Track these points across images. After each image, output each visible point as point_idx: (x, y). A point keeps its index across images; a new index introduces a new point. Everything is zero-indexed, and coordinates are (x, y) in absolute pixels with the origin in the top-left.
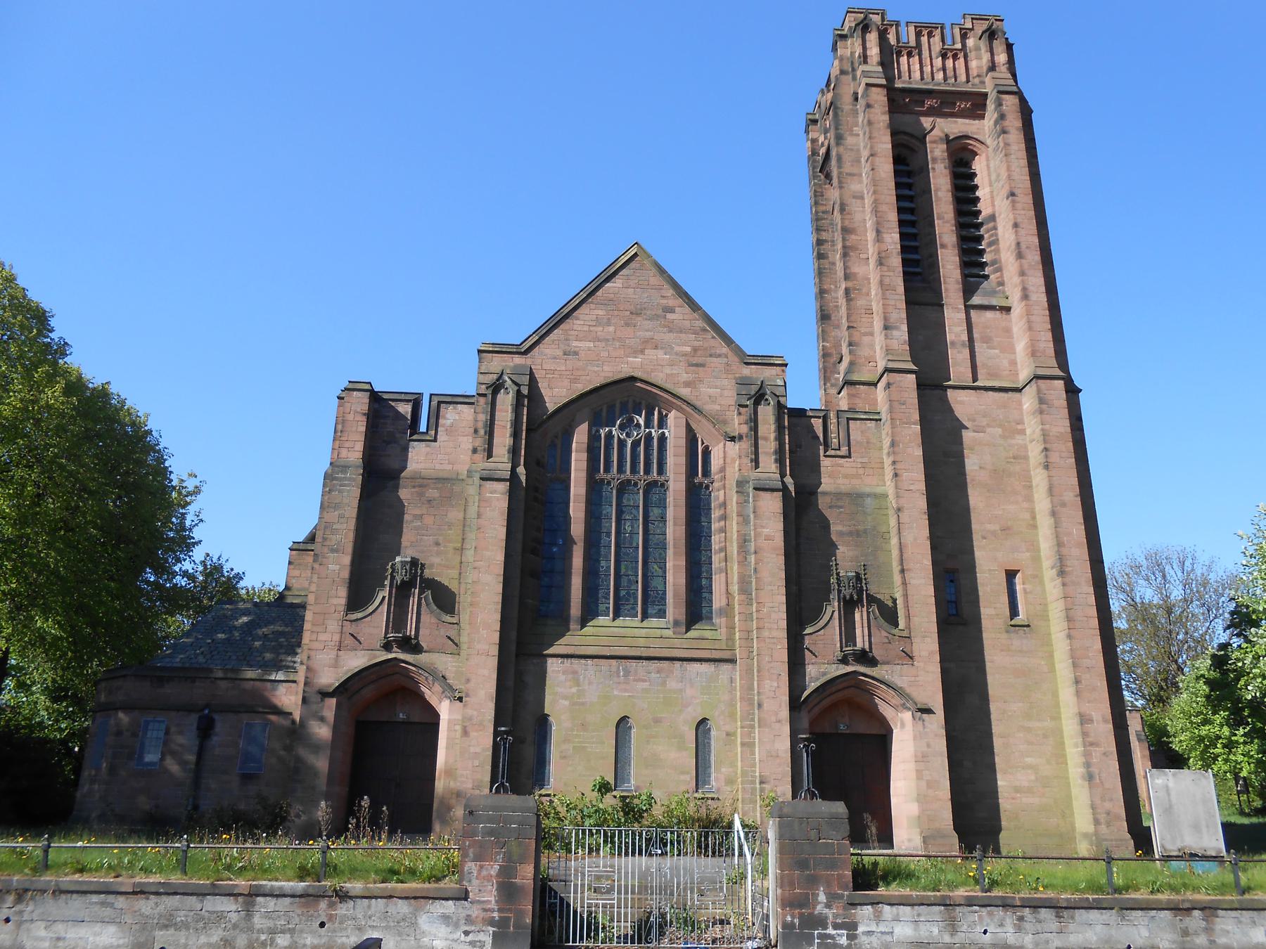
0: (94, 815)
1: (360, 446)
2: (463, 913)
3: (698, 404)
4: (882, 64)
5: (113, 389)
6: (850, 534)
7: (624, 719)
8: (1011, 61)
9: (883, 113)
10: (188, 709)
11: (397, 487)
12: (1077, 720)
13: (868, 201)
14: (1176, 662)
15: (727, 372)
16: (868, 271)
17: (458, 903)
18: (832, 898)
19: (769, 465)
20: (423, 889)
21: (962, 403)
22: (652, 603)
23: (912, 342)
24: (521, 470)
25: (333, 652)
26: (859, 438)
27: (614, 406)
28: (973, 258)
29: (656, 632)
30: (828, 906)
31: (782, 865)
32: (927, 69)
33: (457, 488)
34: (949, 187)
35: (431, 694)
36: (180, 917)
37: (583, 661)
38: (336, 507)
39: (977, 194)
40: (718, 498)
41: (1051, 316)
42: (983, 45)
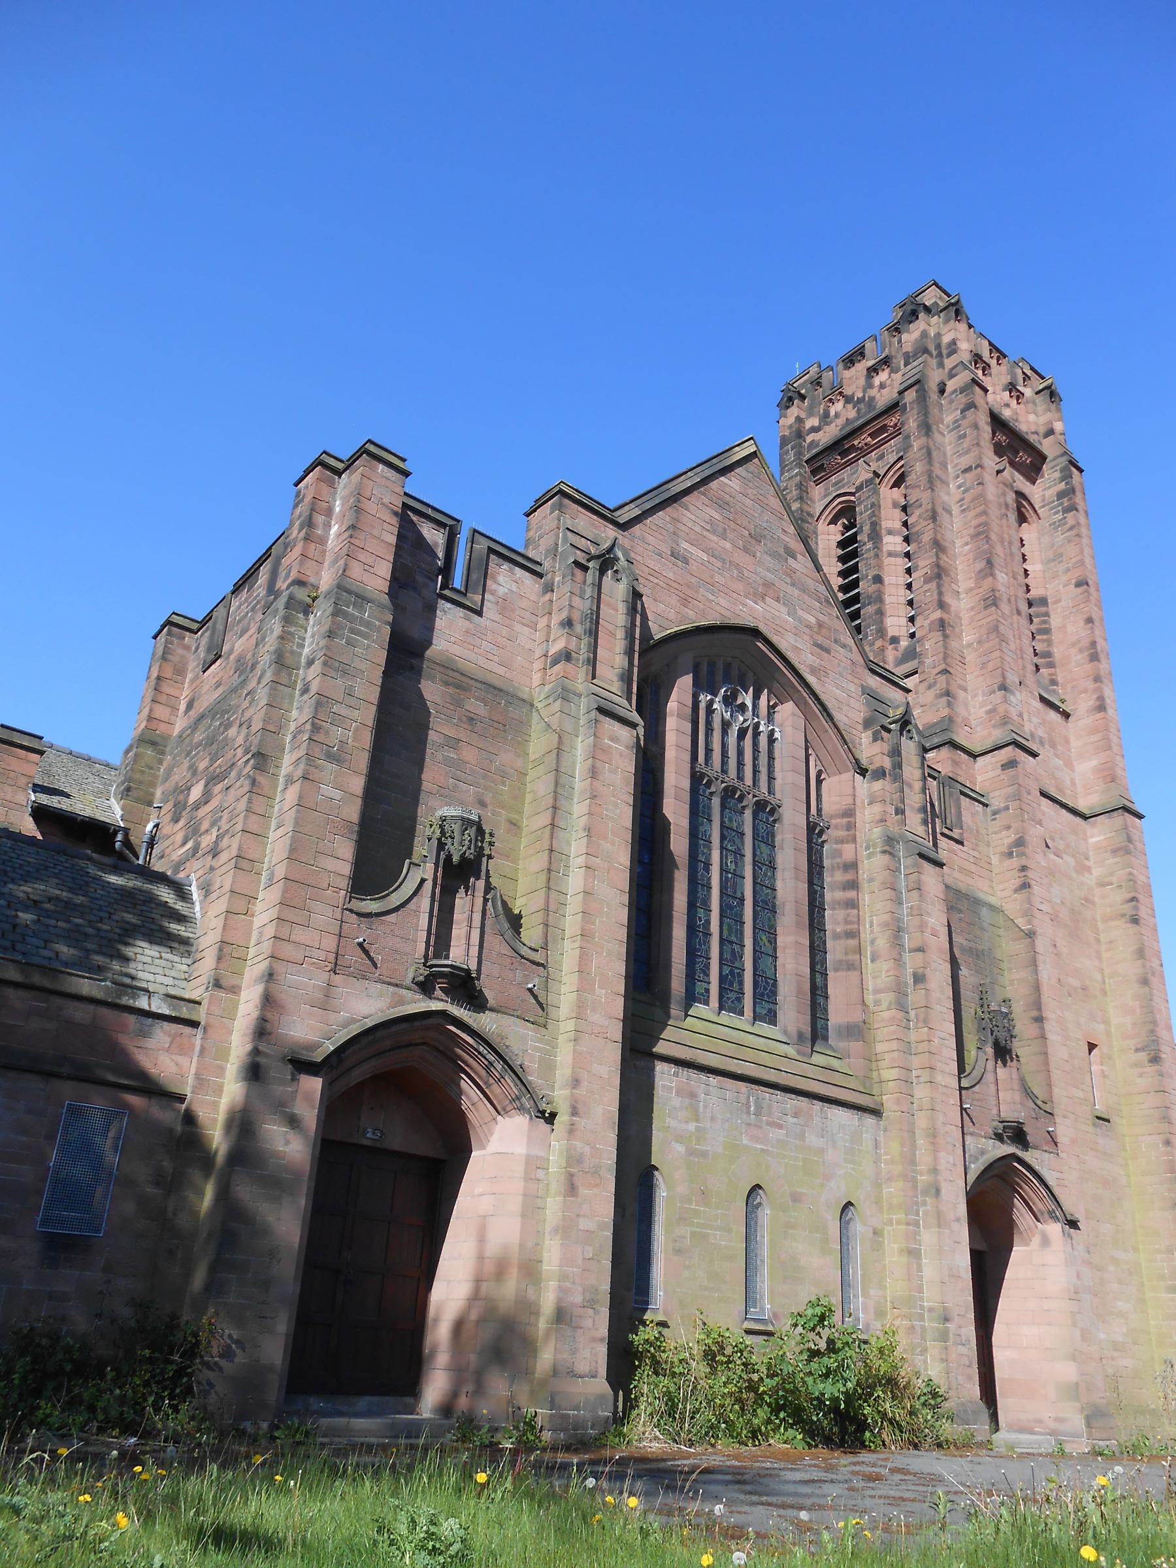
7: (758, 1186)
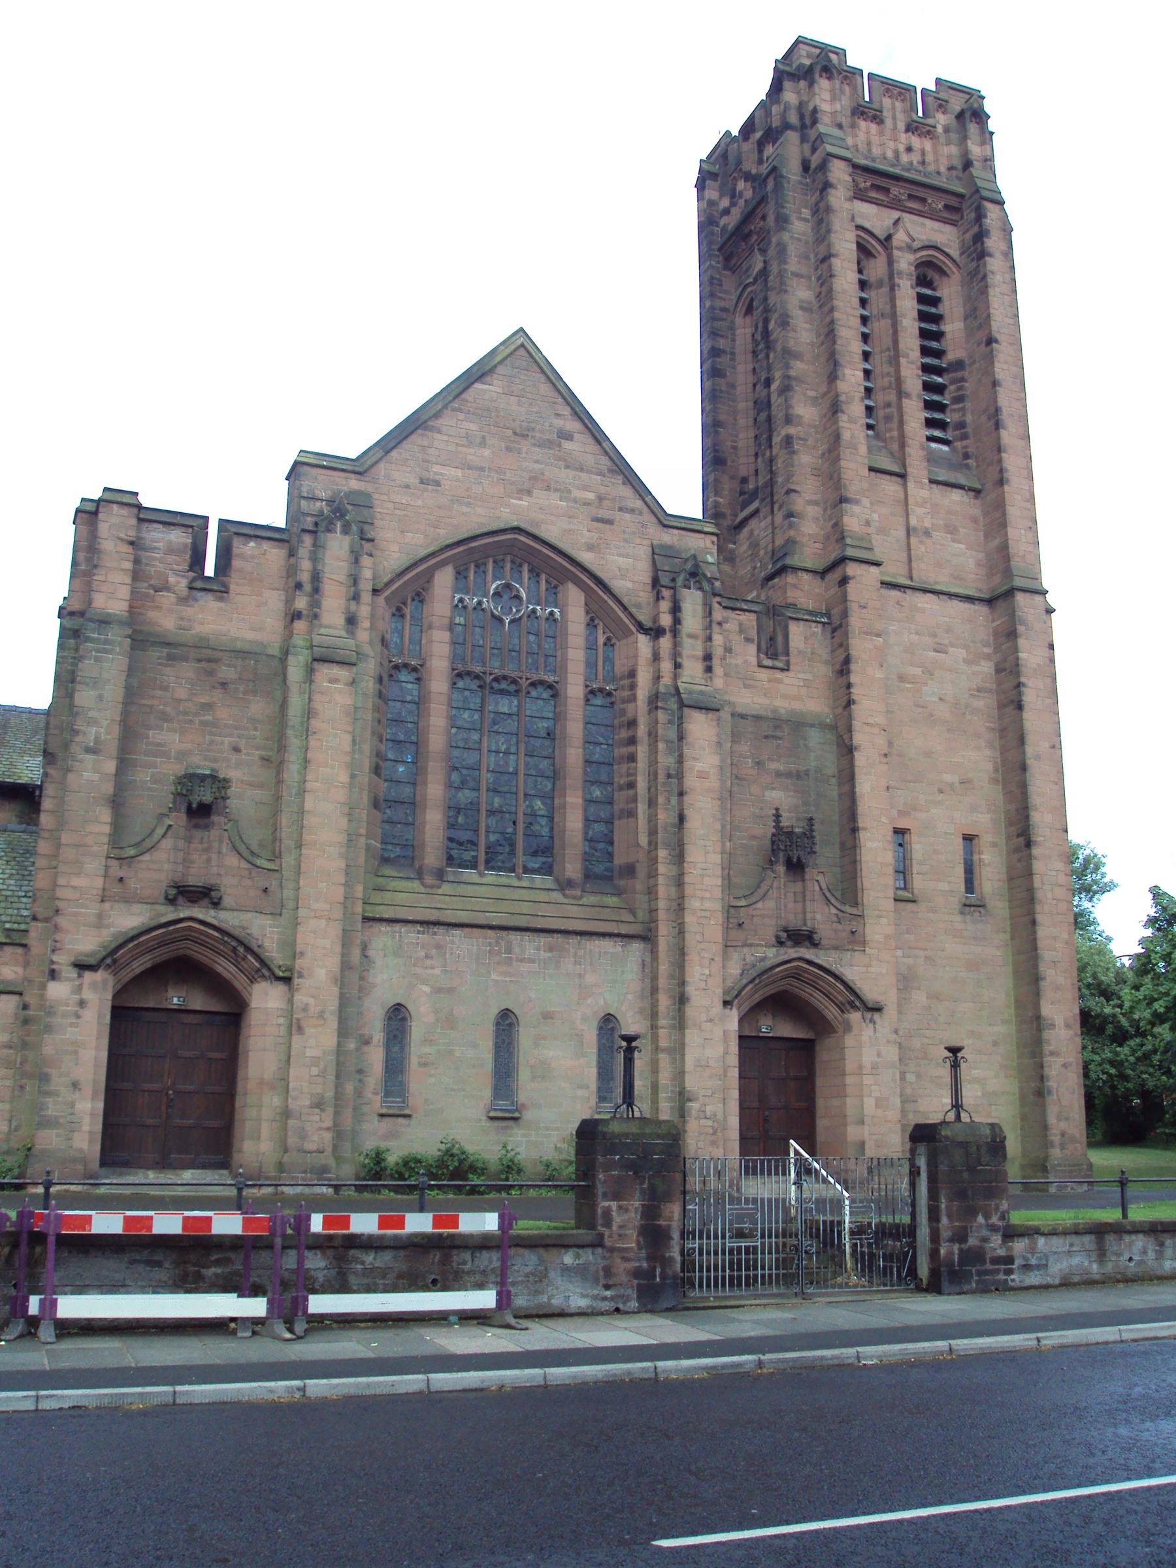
6: (789, 775)
26: (802, 646)
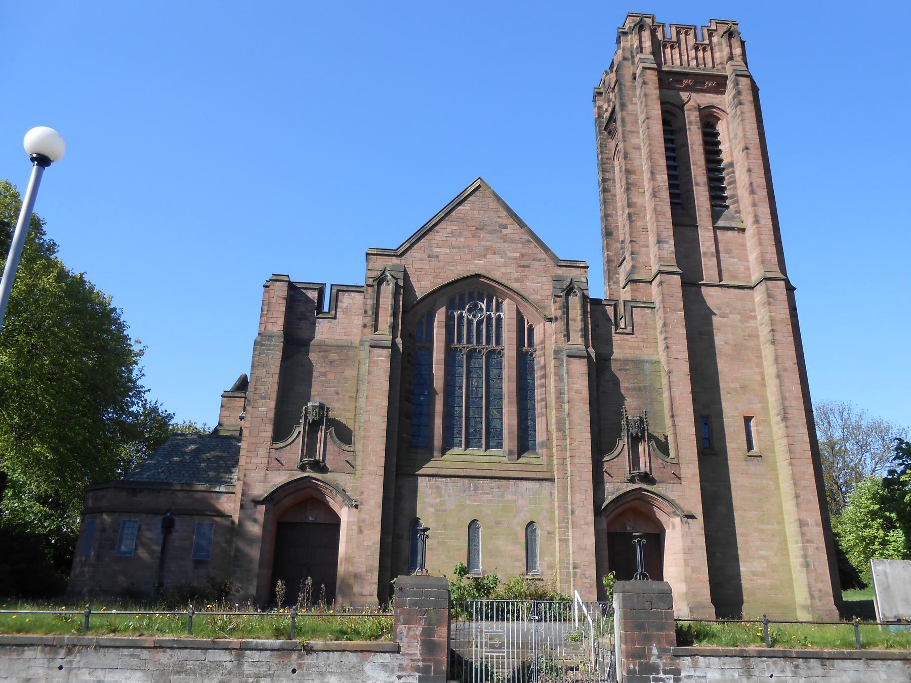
0: (85, 590)
1: (281, 322)
2: (396, 663)
3: (525, 294)
4: (653, 53)
5: (86, 278)
6: (635, 389)
7: (474, 522)
8: (744, 53)
9: (655, 89)
10: (155, 512)
11: (307, 352)
12: (797, 524)
13: (644, 151)
14: (837, 483)
15: (546, 272)
16: (645, 201)
17: (393, 655)
18: (662, 652)
19: (577, 339)
20: (367, 645)
21: (712, 297)
22: (493, 438)
23: (677, 252)
24: (399, 340)
25: (262, 471)
27: (464, 295)
28: (718, 193)
29: (497, 458)
30: (659, 657)
31: (625, 627)
32: (685, 58)
33: (351, 353)
34: (701, 142)
35: (334, 503)
36: (189, 665)
37: (444, 479)
38: (264, 365)
39: (720, 147)
40: (539, 362)
41: (775, 235)
42: (724, 41)
